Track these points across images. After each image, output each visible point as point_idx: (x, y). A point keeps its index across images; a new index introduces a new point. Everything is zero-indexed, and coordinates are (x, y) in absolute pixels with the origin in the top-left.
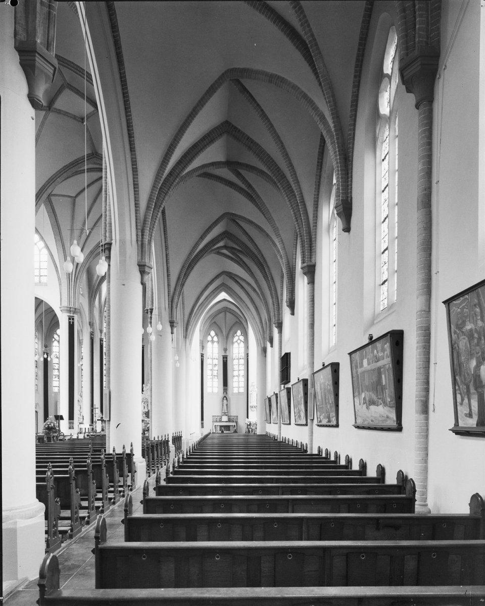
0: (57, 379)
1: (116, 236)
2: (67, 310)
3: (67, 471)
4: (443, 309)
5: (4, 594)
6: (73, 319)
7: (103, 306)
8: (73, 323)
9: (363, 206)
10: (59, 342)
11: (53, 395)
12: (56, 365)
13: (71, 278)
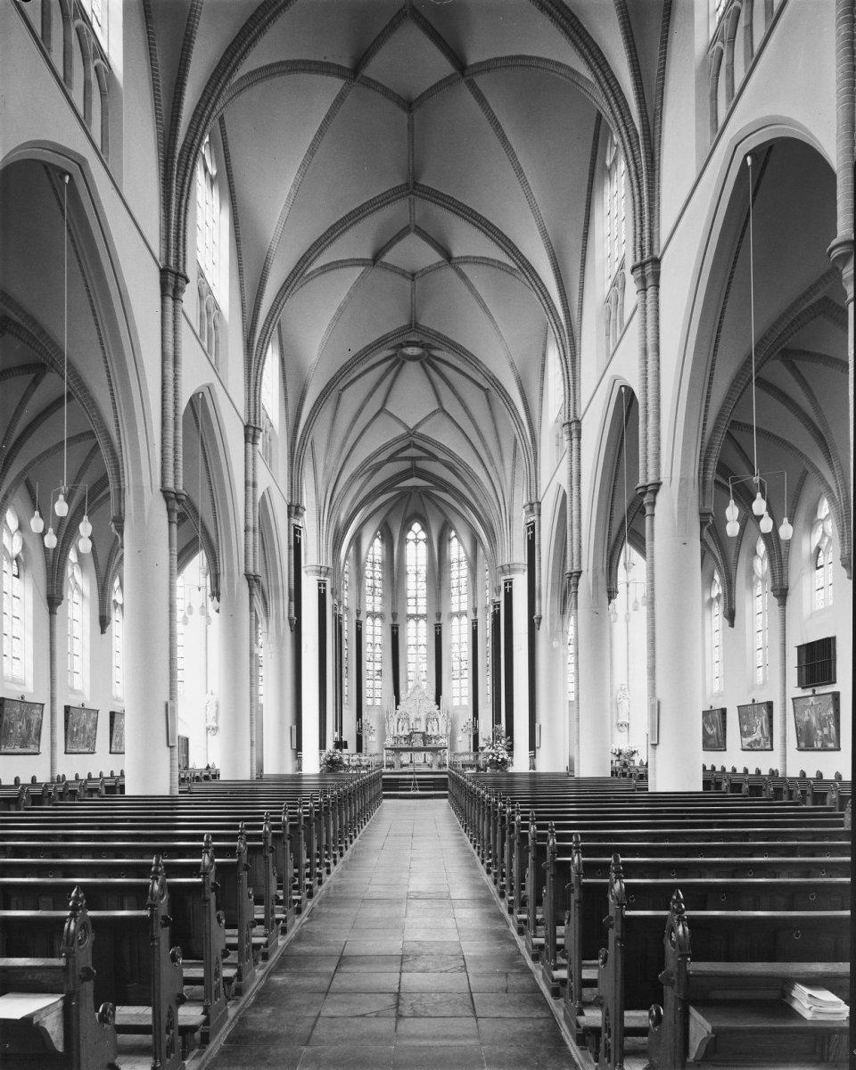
1: (176, 477)
2: (317, 571)
3: (260, 835)
4: (791, 701)
5: (852, 260)
6: (325, 585)
8: (325, 591)
9: (697, 151)
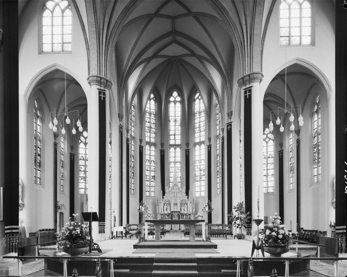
0: (83, 181)
6: (104, 94)
7: (129, 105)
8: (104, 98)
10: (86, 144)
11: (79, 196)
12: (82, 167)
13: (101, 40)
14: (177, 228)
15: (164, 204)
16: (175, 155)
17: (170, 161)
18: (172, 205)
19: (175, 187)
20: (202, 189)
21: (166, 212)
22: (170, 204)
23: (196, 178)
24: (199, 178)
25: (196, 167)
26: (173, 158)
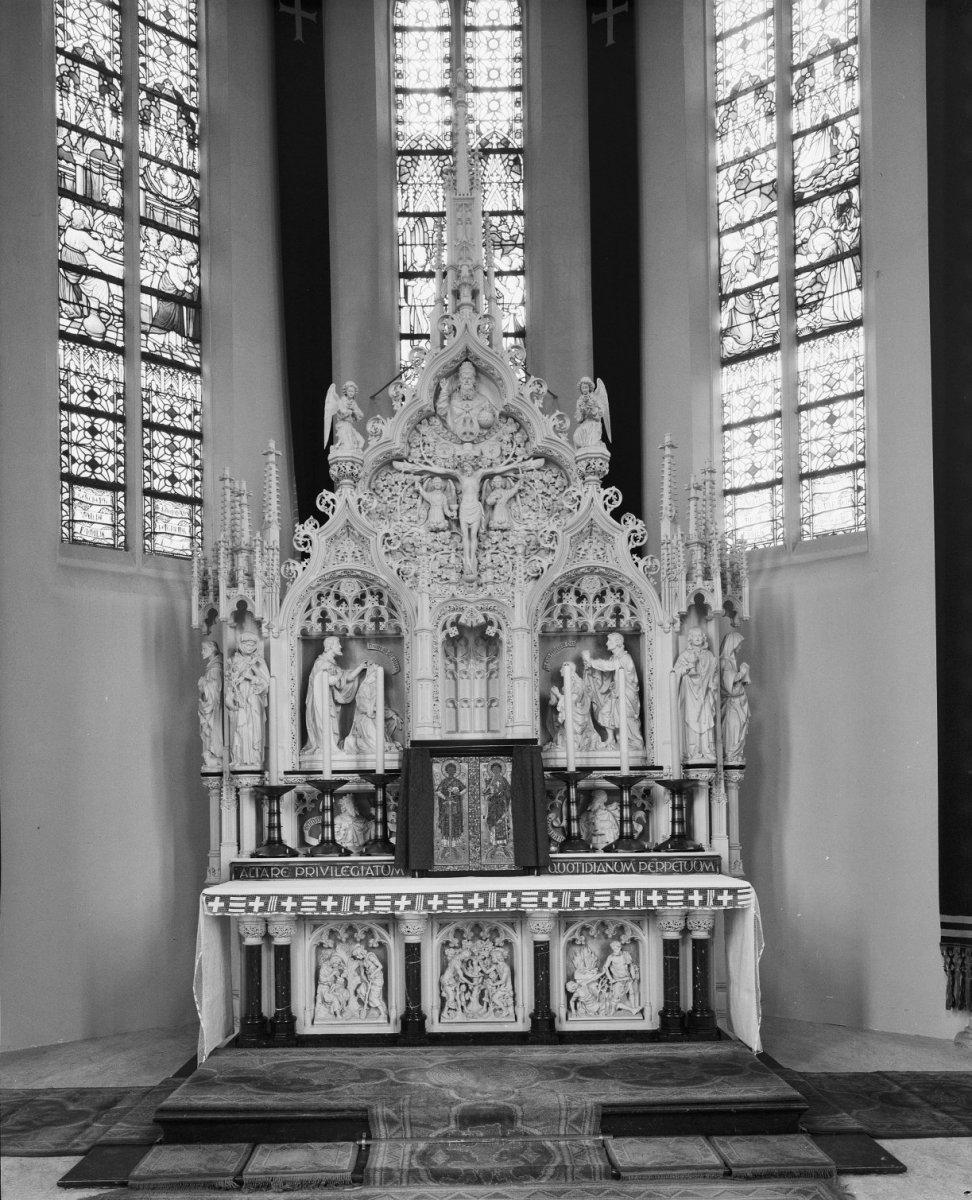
14: (500, 995)
15: (312, 646)
16: (457, 60)
17: (401, 145)
18: (424, 656)
19: (457, 402)
20: (818, 448)
21: (332, 758)
22: (398, 639)
23: (723, 321)
24: (775, 305)
25: (723, 187)
26: (432, 97)
